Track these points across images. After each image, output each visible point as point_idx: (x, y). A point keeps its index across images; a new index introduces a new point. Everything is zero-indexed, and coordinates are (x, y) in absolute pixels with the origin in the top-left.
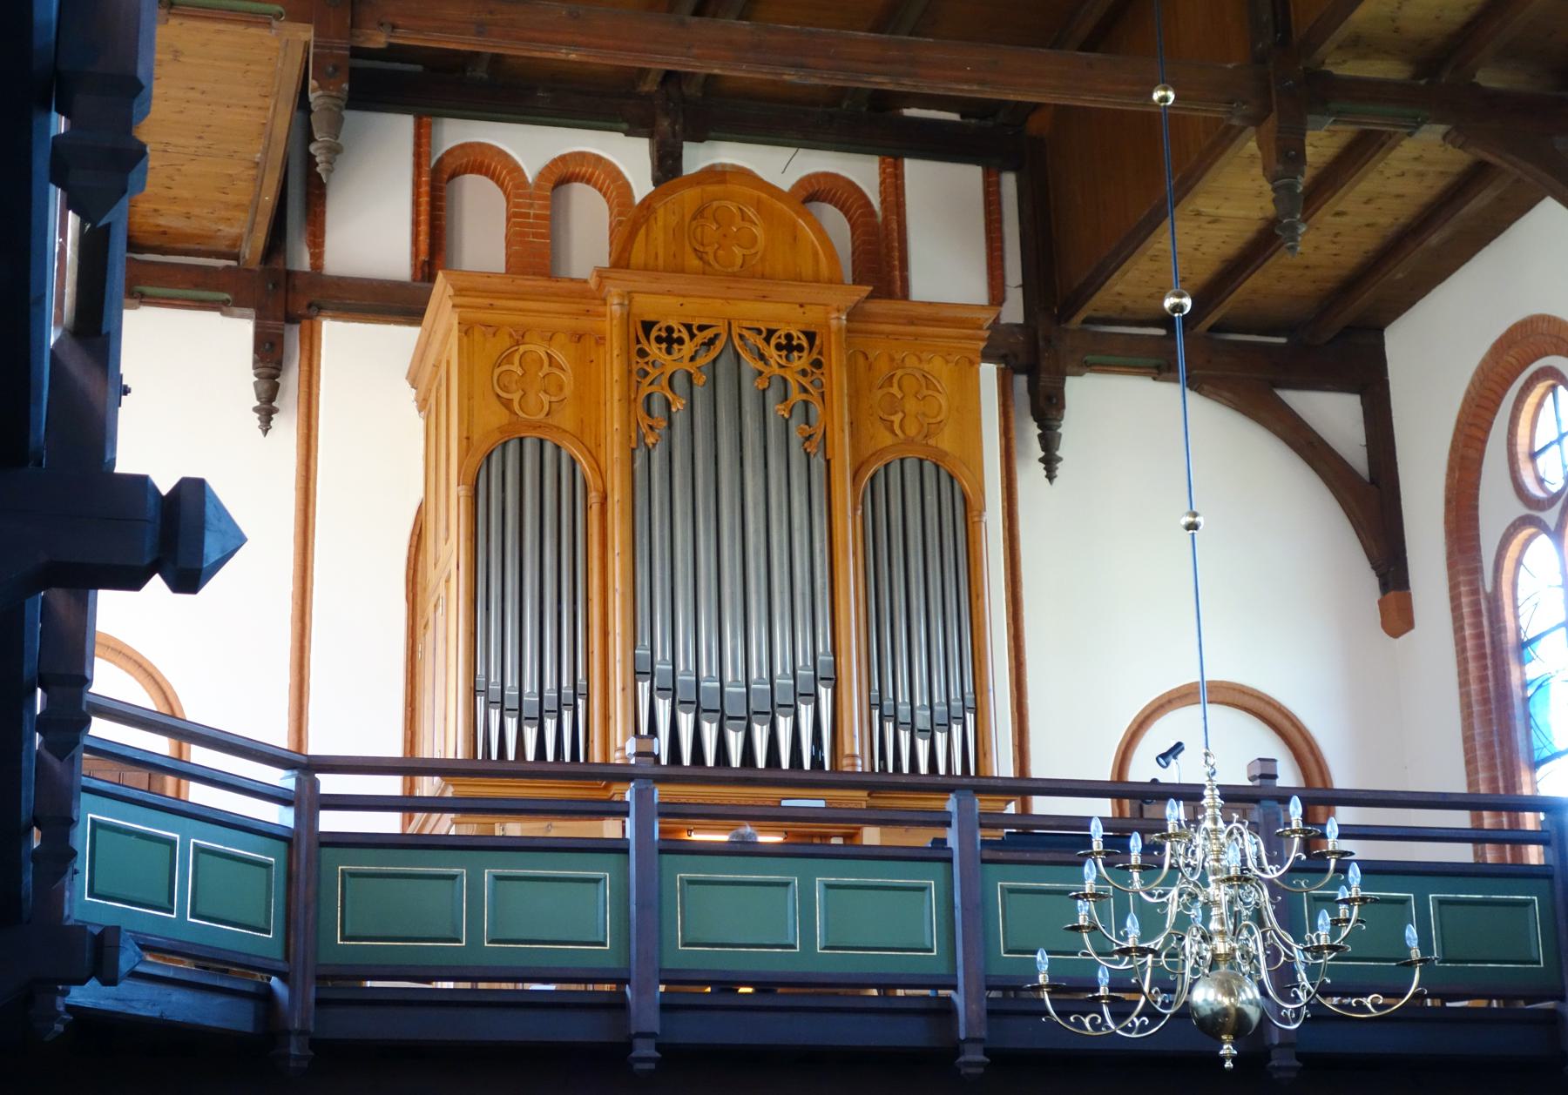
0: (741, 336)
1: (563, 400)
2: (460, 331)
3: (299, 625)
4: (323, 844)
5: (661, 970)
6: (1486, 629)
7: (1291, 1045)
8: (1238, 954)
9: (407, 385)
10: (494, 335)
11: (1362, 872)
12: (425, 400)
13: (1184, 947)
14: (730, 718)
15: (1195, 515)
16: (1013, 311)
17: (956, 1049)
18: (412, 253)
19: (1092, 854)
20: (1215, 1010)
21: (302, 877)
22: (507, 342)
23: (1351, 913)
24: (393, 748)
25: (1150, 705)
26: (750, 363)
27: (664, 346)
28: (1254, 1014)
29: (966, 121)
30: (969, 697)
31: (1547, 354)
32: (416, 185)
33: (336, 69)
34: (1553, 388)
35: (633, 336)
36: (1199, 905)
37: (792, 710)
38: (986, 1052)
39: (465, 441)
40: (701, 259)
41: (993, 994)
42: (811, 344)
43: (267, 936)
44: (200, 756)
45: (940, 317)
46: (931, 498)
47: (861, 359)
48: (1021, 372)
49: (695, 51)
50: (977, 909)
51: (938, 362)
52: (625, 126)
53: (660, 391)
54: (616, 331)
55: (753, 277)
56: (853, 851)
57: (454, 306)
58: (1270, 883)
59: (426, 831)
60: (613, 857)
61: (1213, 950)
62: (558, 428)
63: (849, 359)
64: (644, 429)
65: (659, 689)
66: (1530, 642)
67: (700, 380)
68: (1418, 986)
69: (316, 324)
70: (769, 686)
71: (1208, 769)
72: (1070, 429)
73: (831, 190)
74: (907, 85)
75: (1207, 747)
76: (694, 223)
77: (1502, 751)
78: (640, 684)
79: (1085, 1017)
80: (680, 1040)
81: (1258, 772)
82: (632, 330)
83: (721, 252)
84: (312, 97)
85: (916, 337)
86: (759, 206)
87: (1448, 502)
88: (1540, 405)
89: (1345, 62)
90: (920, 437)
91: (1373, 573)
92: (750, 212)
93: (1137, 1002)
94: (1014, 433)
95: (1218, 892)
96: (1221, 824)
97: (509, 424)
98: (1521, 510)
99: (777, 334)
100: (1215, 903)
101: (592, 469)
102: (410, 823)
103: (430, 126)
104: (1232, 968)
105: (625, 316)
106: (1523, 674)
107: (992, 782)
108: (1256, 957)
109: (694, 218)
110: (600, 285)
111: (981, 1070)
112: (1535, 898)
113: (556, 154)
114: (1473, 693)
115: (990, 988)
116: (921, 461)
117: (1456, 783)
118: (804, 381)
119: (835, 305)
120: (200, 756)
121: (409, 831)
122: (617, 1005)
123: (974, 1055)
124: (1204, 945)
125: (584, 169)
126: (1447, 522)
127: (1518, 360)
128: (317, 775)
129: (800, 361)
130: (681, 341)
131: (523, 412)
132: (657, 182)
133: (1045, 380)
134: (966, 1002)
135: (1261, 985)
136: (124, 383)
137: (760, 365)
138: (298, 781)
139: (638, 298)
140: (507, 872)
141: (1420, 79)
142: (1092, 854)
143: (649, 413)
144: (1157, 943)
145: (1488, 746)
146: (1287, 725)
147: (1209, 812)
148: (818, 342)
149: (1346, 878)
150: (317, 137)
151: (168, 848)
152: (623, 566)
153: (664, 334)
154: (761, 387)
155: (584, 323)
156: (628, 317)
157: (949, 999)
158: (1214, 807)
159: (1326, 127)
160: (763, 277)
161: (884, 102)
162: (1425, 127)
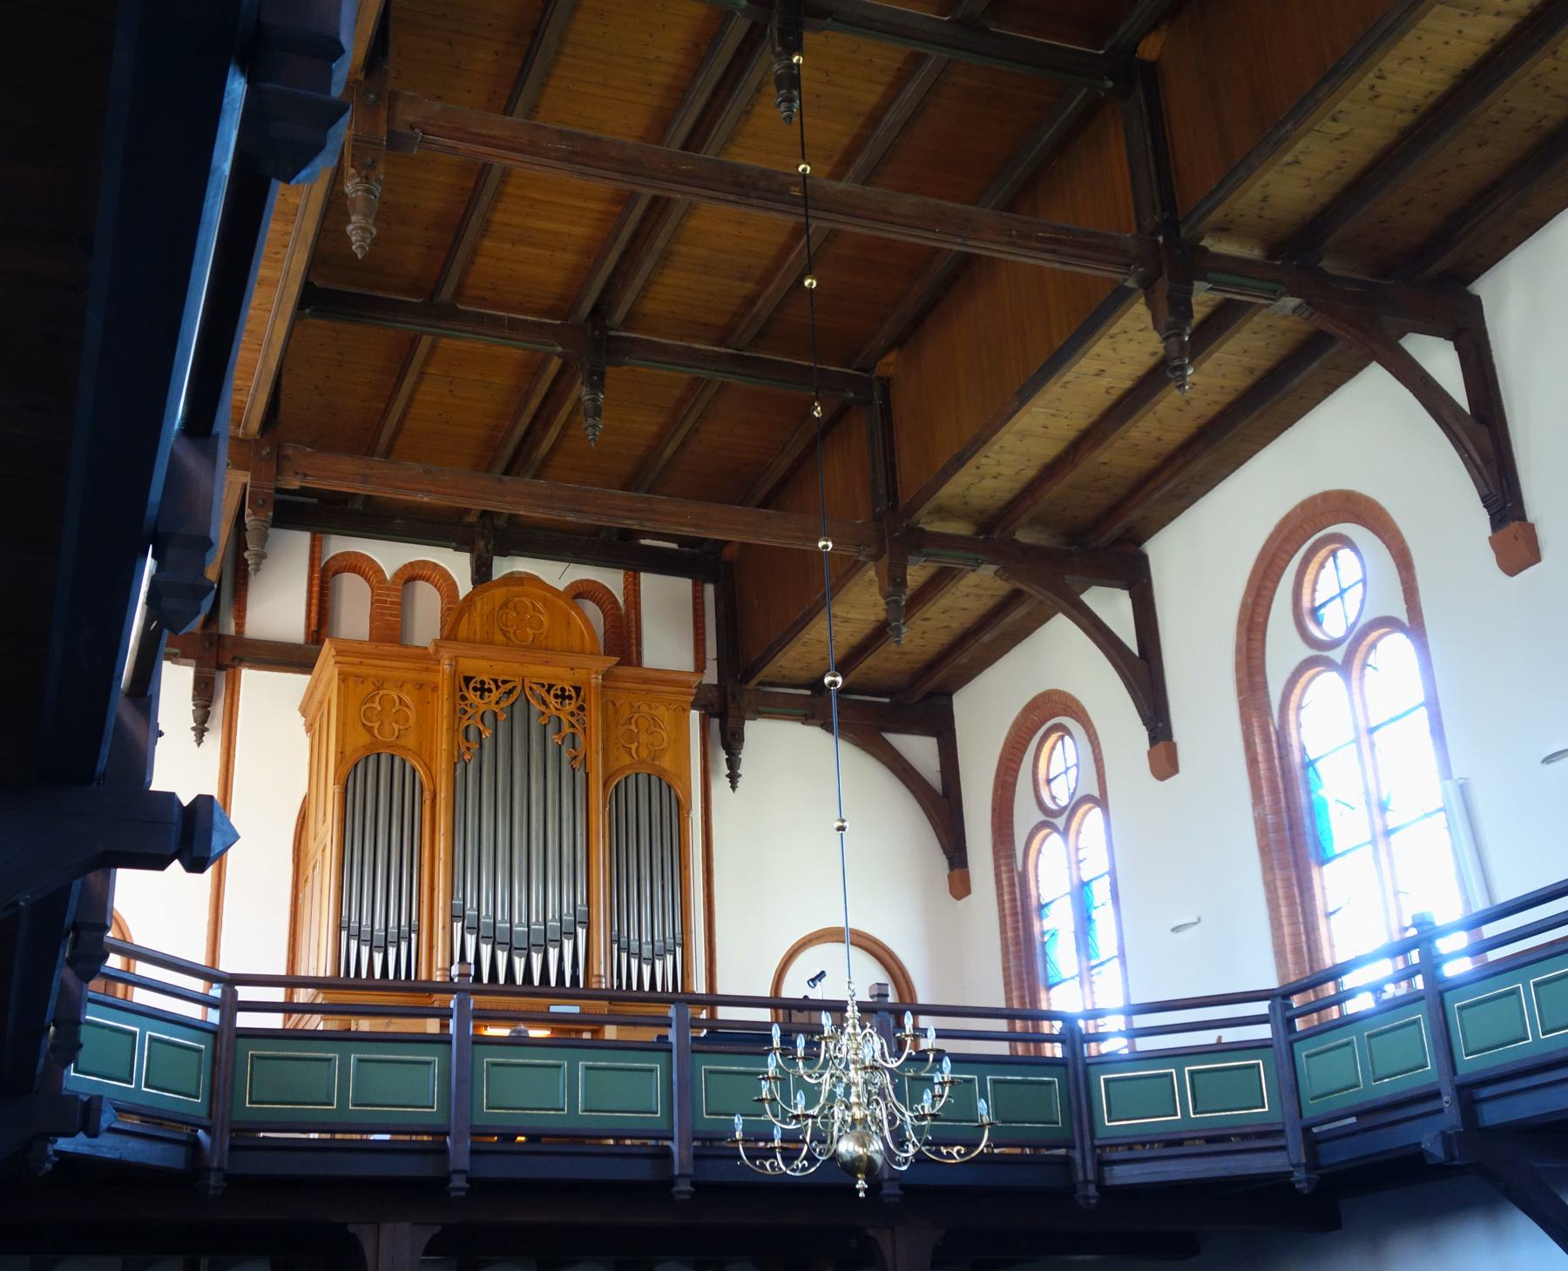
0: (531, 688)
1: (408, 729)
2: (339, 679)
3: (217, 879)
4: (239, 1036)
5: (471, 1126)
6: (1018, 896)
7: (896, 1179)
8: (869, 1118)
9: (298, 714)
10: (363, 682)
11: (951, 1061)
12: (311, 725)
13: (833, 1112)
14: (516, 949)
15: (843, 821)
16: (711, 676)
17: (671, 1182)
18: (306, 624)
19: (773, 1049)
20: (854, 1156)
21: (223, 1059)
22: (371, 688)
23: (943, 1091)
24: (280, 970)
25: (797, 943)
26: (536, 707)
27: (478, 693)
28: (879, 1159)
29: (681, 549)
30: (678, 936)
31: (1058, 715)
32: (311, 579)
33: (265, 502)
34: (1062, 738)
35: (457, 687)
36: (844, 1085)
37: (559, 944)
38: (692, 1184)
39: (340, 755)
40: (505, 635)
41: (695, 1143)
42: (578, 695)
43: (196, 1100)
44: (143, 969)
45: (664, 679)
46: (655, 800)
47: (611, 707)
48: (716, 717)
49: (508, 499)
50: (689, 1084)
51: (662, 709)
52: (454, 544)
53: (475, 723)
54: (446, 682)
55: (540, 649)
56: (598, 1044)
57: (336, 663)
58: (890, 1070)
59: (300, 1027)
60: (441, 1047)
61: (853, 1117)
62: (404, 747)
63: (603, 705)
64: (463, 750)
65: (468, 928)
66: (1047, 905)
67: (502, 717)
68: (987, 1141)
69: (237, 672)
70: (543, 927)
71: (850, 992)
72: (746, 755)
73: (591, 591)
74: (648, 526)
75: (850, 977)
76: (501, 612)
77: (1028, 977)
78: (455, 924)
79: (766, 1161)
80: (483, 1175)
81: (876, 993)
82: (457, 683)
83: (518, 631)
84: (247, 520)
85: (648, 692)
86: (545, 601)
87: (994, 810)
88: (1053, 748)
89: (932, 522)
90: (649, 759)
91: (944, 856)
92: (539, 606)
93: (802, 1150)
94: (710, 757)
95: (856, 1076)
96: (858, 1030)
97: (371, 743)
98: (1041, 817)
99: (555, 688)
100: (854, 1083)
101: (426, 775)
102: (289, 1020)
103: (321, 539)
104: (864, 1128)
105: (453, 673)
106: (1042, 926)
107: (695, 997)
108: (881, 1121)
109: (501, 608)
110: (436, 652)
111: (688, 1197)
112: (1056, 1080)
113: (407, 562)
114: (1009, 938)
115: (695, 1139)
116: (649, 775)
117: (1000, 1003)
118: (573, 720)
119: (595, 669)
120: (143, 969)
121: (287, 1027)
122: (442, 1151)
123: (684, 1186)
124: (846, 1112)
125: (425, 572)
126: (993, 824)
127: (1038, 717)
128: (237, 988)
129: (570, 706)
130: (490, 690)
131: (381, 736)
132: (474, 582)
133: (731, 723)
134: (679, 1150)
135: (883, 1139)
136: (160, 729)
137: (543, 708)
138: (223, 992)
139: (461, 661)
140: (366, 1056)
141: (980, 534)
142: (773, 1049)
143: (467, 739)
144: (814, 1111)
145: (1019, 974)
146: (887, 957)
147: (850, 1021)
148: (582, 693)
149: (941, 1066)
150: (249, 546)
151: (131, 1038)
152: (446, 841)
153: (479, 686)
154: (543, 723)
155: (424, 676)
156: (454, 673)
157: (668, 1147)
158: (854, 1018)
159: (920, 563)
160: (547, 649)
161: (628, 536)
162: (983, 566)
